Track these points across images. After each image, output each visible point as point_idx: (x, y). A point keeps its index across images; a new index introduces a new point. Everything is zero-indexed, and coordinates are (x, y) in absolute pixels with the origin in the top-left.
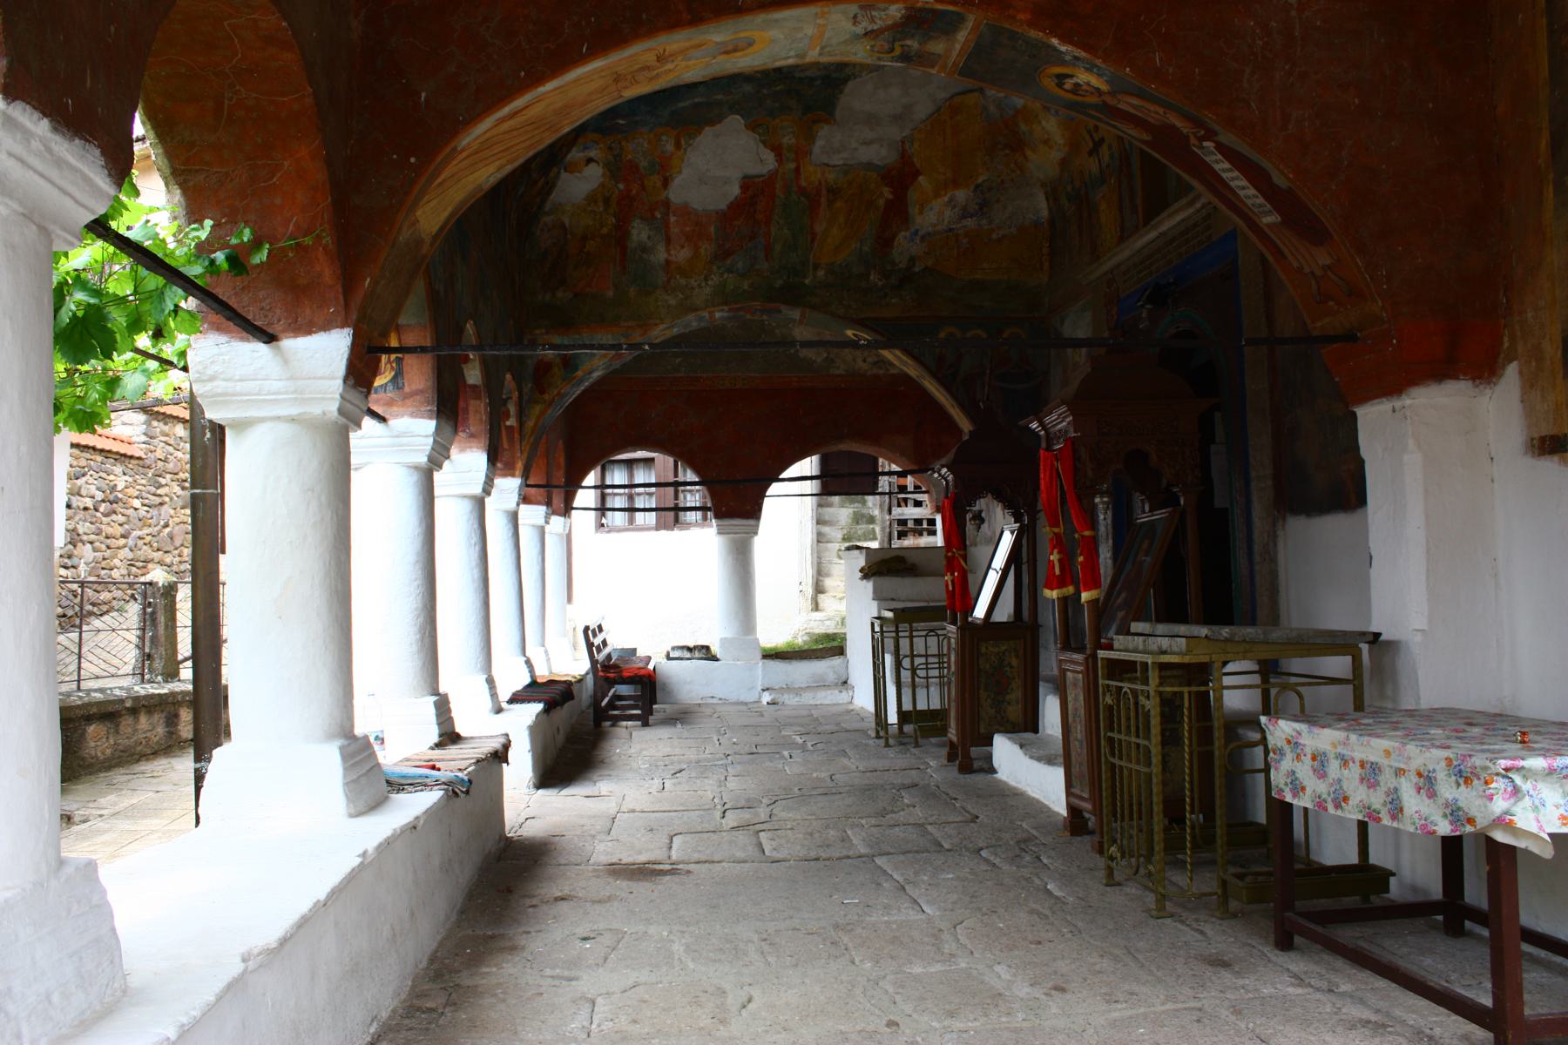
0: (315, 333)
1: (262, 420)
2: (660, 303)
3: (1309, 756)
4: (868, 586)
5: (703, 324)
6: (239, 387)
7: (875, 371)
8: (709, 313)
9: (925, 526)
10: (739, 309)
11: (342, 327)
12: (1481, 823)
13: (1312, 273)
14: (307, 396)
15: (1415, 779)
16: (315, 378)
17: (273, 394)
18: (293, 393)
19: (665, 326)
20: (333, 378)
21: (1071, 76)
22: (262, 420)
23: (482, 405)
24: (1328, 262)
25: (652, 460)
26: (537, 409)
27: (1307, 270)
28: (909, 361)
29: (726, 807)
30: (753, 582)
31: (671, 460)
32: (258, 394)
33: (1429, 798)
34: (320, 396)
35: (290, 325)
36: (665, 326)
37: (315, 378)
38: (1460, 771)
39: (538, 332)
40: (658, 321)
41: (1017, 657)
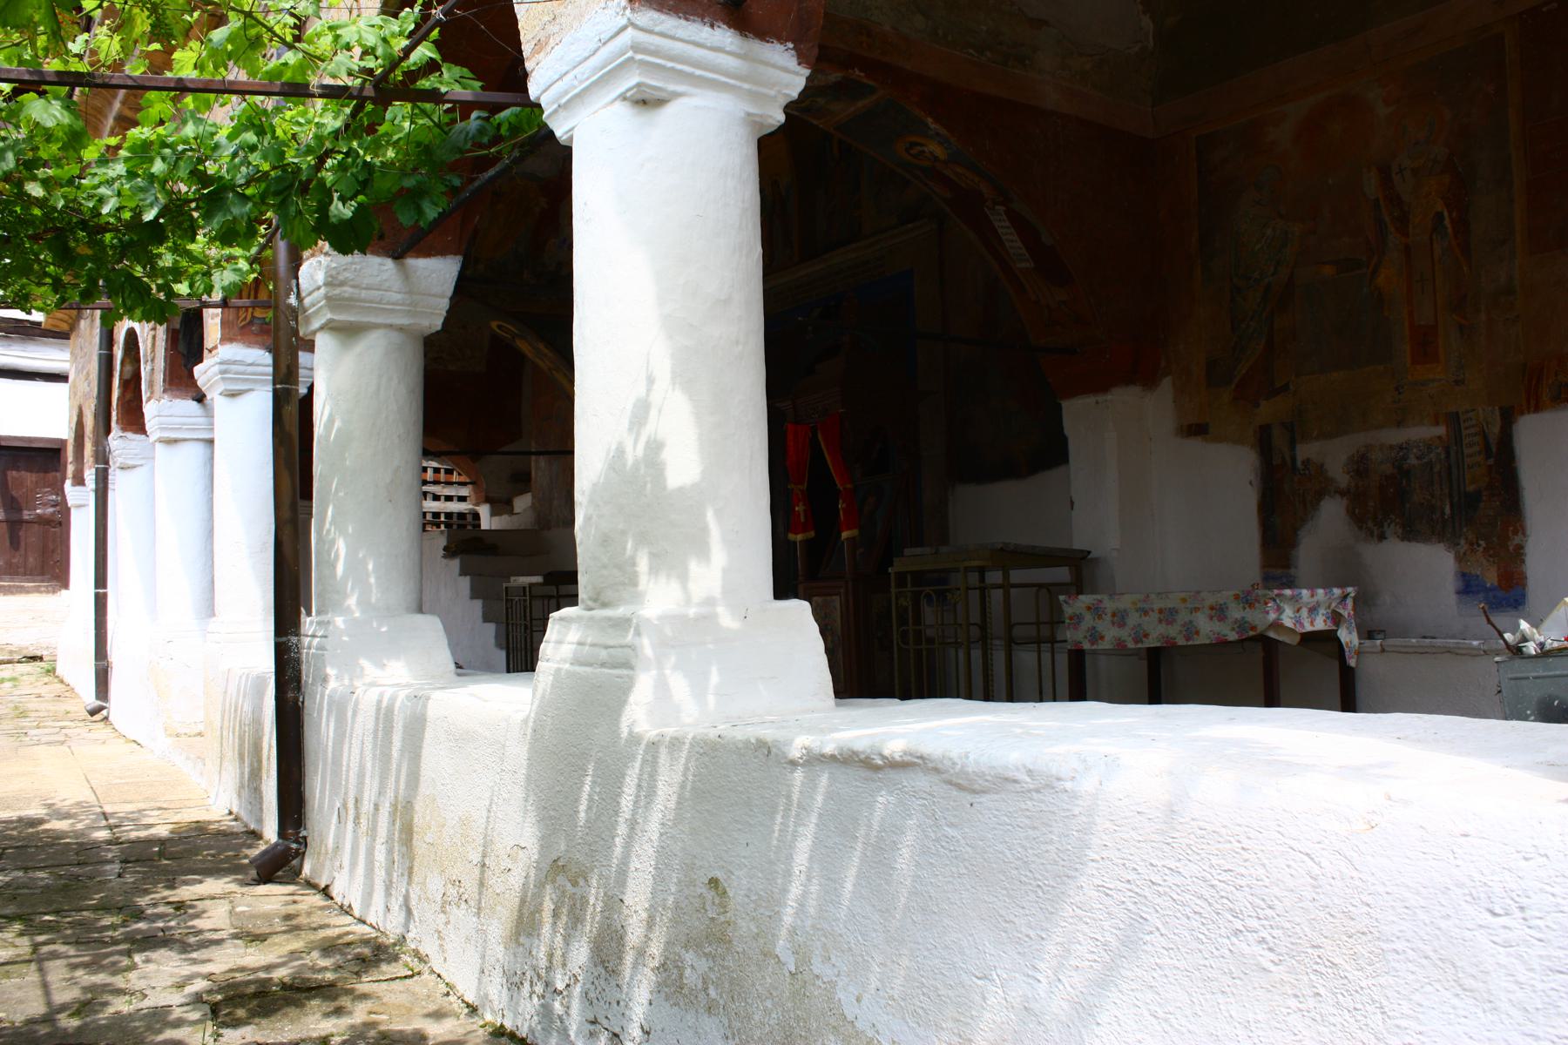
0: (434, 256)
1: (376, 326)
3: (1109, 615)
4: (455, 564)
6: (364, 294)
9: (443, 519)
11: (455, 254)
12: (1260, 629)
15: (1208, 612)
17: (393, 304)
18: (408, 305)
20: (442, 296)
21: (922, 145)
22: (376, 326)
32: (380, 303)
33: (1219, 621)
37: (430, 295)
38: (1247, 600)
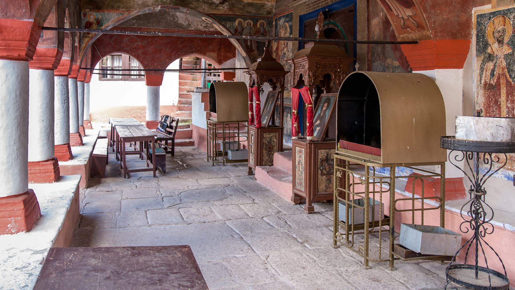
2: (135, 3)
5: (150, 12)
7: (205, 29)
8: (153, 8)
10: (165, 7)
13: (403, 18)
14: (11, 48)
16: (15, 40)
18: (4, 46)
19: (136, 11)
23: (69, 40)
24: (411, 14)
25: (121, 55)
26: (86, 40)
27: (400, 16)
28: (225, 30)
29: (163, 196)
30: (159, 99)
31: (128, 56)
34: (17, 48)
35: (3, 16)
36: (136, 11)
39: (87, 10)
40: (134, 10)
41: (276, 138)
